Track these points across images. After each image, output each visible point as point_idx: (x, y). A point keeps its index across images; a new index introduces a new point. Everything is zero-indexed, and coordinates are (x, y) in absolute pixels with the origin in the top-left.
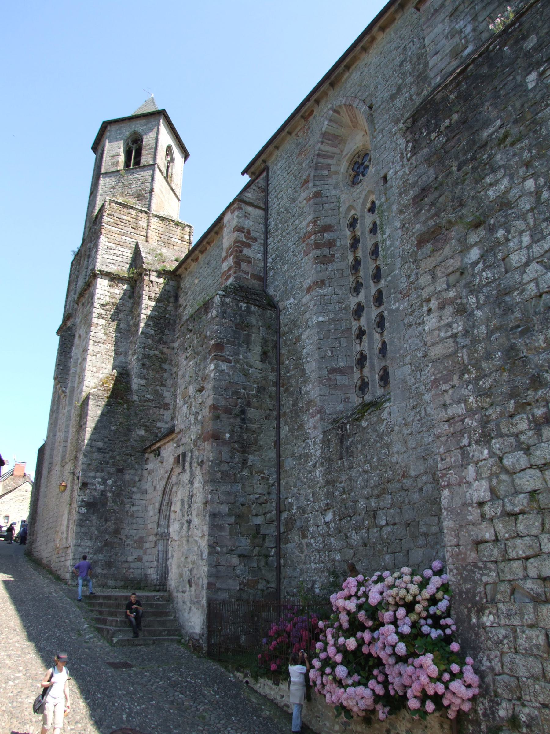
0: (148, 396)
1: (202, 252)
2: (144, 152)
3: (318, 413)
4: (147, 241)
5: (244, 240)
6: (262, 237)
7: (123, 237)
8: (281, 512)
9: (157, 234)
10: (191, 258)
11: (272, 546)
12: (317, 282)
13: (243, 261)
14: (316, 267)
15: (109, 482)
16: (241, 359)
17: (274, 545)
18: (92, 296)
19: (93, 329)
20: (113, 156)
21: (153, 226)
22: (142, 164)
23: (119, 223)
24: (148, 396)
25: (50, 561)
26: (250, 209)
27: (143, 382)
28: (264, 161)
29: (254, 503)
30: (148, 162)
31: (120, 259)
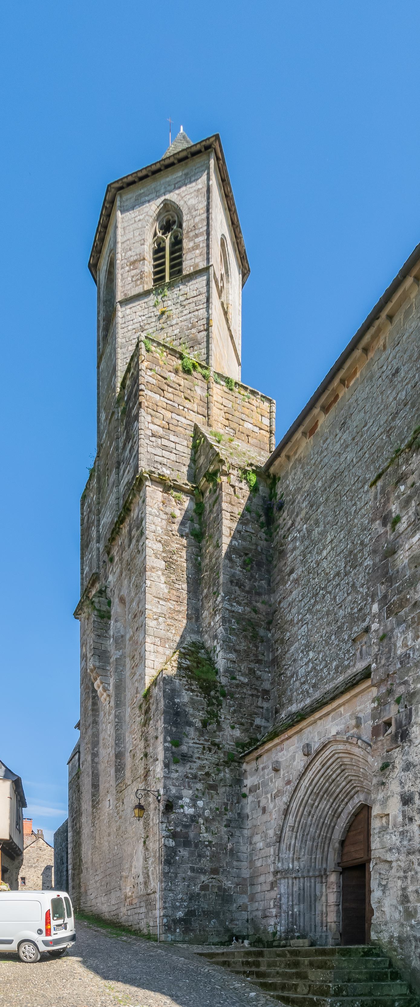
0: (242, 678)
1: (326, 409)
2: (187, 244)
7: (174, 415)
9: (222, 413)
10: (302, 429)
15: (200, 803)
18: (140, 524)
19: (148, 573)
20: (133, 263)
22: (185, 273)
23: (166, 387)
24: (242, 678)
25: (117, 915)
27: (233, 656)
30: (197, 265)
31: (173, 457)
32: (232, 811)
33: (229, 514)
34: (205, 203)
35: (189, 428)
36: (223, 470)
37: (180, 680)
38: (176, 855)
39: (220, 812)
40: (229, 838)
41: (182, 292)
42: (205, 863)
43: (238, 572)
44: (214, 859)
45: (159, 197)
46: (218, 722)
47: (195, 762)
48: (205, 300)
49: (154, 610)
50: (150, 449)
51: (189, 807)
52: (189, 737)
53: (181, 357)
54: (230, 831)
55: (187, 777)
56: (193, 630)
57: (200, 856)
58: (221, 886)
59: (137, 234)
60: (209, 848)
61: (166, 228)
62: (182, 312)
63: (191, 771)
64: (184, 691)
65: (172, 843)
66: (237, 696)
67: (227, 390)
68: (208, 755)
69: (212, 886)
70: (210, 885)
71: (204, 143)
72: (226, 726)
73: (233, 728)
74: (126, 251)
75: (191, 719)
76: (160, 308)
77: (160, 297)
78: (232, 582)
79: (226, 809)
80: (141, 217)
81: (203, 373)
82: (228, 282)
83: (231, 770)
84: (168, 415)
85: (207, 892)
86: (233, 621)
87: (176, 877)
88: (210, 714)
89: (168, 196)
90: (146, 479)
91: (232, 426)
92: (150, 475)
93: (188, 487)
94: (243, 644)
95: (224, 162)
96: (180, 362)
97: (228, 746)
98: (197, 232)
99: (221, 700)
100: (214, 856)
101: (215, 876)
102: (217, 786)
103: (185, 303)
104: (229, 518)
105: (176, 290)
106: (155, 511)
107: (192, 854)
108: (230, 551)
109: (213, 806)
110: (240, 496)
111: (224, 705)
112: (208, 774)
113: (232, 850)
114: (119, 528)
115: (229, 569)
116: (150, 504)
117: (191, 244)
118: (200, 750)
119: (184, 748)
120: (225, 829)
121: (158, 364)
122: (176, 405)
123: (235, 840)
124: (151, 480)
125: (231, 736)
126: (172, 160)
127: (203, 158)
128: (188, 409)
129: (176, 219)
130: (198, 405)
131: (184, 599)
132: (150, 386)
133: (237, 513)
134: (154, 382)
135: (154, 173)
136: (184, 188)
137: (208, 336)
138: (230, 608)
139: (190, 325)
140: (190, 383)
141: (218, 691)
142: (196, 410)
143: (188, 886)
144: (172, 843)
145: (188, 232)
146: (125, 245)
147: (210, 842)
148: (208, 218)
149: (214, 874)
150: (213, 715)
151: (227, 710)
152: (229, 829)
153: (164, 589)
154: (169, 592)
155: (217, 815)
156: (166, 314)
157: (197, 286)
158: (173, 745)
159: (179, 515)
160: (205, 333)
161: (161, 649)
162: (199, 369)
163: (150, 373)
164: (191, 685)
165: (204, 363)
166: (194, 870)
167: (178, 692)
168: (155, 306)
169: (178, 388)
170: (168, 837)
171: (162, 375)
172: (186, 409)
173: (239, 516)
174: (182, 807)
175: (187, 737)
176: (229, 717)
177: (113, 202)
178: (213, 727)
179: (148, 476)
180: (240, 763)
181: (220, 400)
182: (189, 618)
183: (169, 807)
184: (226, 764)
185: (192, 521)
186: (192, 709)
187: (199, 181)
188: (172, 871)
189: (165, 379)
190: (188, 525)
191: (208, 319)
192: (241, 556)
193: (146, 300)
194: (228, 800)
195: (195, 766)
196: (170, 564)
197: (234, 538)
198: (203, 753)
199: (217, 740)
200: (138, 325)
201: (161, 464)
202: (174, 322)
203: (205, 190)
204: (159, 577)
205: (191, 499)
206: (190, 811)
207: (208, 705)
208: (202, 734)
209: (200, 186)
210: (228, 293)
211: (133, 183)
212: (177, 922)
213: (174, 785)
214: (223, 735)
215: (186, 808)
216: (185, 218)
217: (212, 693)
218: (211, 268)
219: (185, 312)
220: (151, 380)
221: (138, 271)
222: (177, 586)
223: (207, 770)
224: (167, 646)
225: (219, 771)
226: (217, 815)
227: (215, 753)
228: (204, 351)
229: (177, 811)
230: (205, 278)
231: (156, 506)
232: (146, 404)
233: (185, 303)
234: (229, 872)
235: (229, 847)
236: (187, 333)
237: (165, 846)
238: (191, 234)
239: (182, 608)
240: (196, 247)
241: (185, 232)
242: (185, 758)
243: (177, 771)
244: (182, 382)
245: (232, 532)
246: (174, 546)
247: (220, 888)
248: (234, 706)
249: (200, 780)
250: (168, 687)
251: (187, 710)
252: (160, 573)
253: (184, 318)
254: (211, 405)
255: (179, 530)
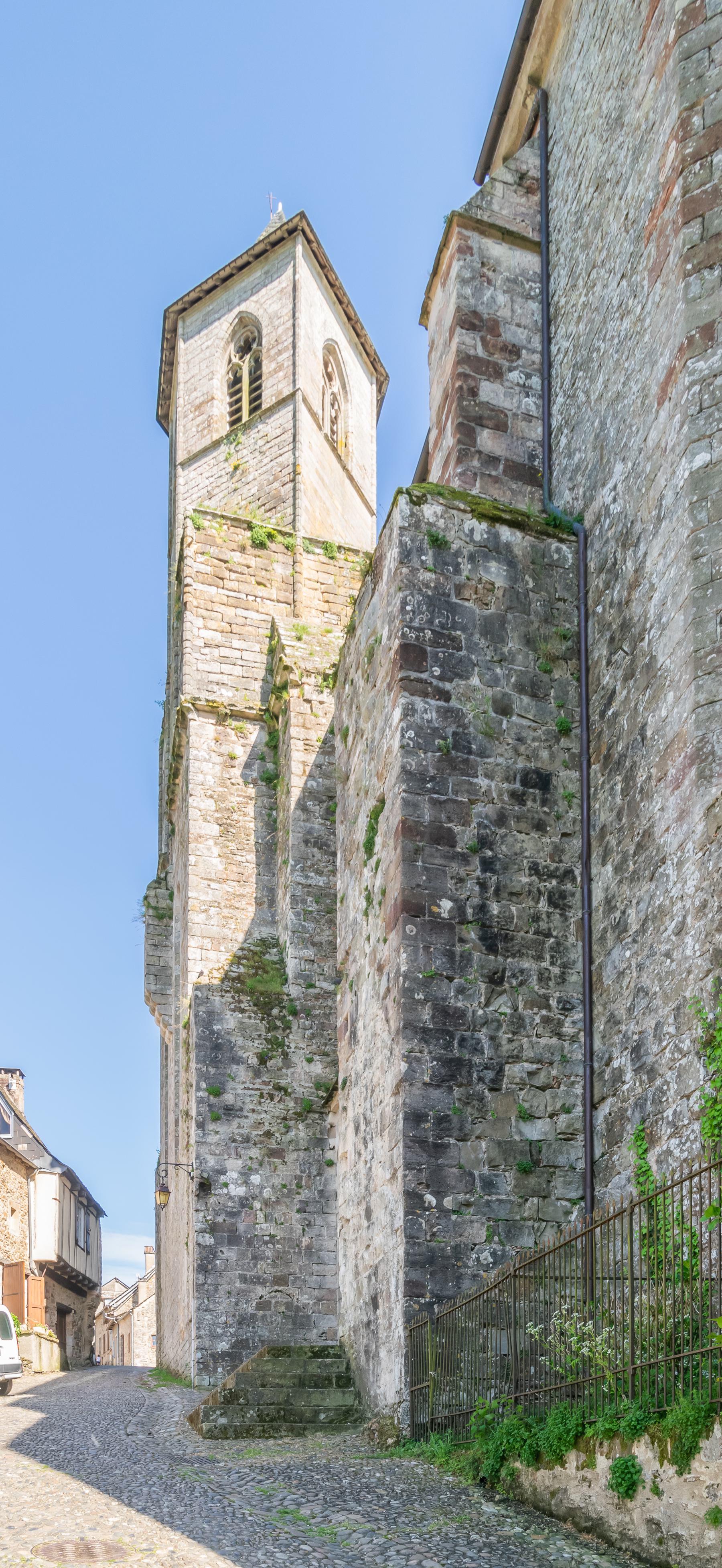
2: (267, 367)
3: (691, 765)
4: (296, 616)
5: (480, 352)
6: (537, 343)
7: (240, 612)
8: (594, 1107)
9: (318, 594)
11: (574, 1195)
12: (691, 339)
13: (480, 421)
14: (687, 286)
15: (255, 1179)
16: (475, 689)
17: (580, 1193)
19: (192, 846)
20: (199, 407)
21: (305, 574)
23: (227, 574)
26: (497, 250)
27: (310, 953)
28: (535, 81)
29: (522, 1085)
30: (280, 392)
31: (238, 671)
32: (308, 1188)
33: (302, 743)
34: (291, 306)
35: (263, 625)
36: (292, 681)
37: (223, 996)
38: (215, 1256)
39: (290, 1191)
40: (304, 1230)
41: (261, 434)
42: (264, 1268)
43: (317, 826)
44: (278, 1262)
45: (230, 310)
46: (285, 1055)
47: (246, 1117)
48: (291, 439)
49: (202, 898)
50: (201, 666)
51: (237, 1184)
52: (237, 1080)
53: (250, 527)
54: (305, 1219)
55: (234, 1141)
56: (264, 920)
57: (255, 1258)
58: (292, 1303)
59: (203, 366)
60: (270, 1246)
61: (245, 349)
62: (261, 461)
63: (240, 1131)
64: (229, 1013)
65: (209, 1240)
66: (317, 1012)
67: (325, 560)
68: (268, 1105)
69: (277, 1302)
70: (273, 1301)
71: (286, 227)
72: (297, 1058)
73: (310, 1061)
74: (189, 392)
75: (240, 1053)
76: (233, 462)
77: (233, 446)
78: (306, 842)
79: (299, 1186)
80: (209, 343)
81: (286, 542)
82: (346, 400)
83: (308, 1126)
84: (230, 612)
85: (268, 1313)
86: (310, 899)
87: (216, 1290)
88: (272, 1044)
89: (243, 307)
90: (189, 709)
91: (333, 610)
92: (193, 704)
93: (254, 712)
94: (327, 933)
95: (319, 244)
96: (249, 534)
97: (302, 1090)
98: (280, 347)
99: (289, 1021)
100: (279, 1258)
101: (280, 1288)
102: (283, 1150)
103: (264, 448)
104: (302, 748)
105: (253, 433)
106: (203, 754)
107: (242, 1255)
108: (304, 797)
109: (277, 1181)
110: (321, 713)
111: (294, 1028)
112: (268, 1134)
113: (309, 1247)
114: (175, 784)
115: (302, 824)
116: (196, 745)
117: (273, 365)
118: (256, 1099)
119: (229, 1098)
120: (298, 1216)
121: (214, 544)
122: (244, 596)
123: (315, 1231)
124: (197, 710)
125: (306, 1073)
126: (245, 258)
127: (289, 244)
128: (262, 598)
129: (256, 334)
130: (279, 589)
131: (250, 876)
132: (201, 576)
133: (315, 739)
134: (209, 569)
135: (225, 280)
136: (264, 291)
137: (294, 489)
138: (303, 881)
139: (271, 478)
140: (266, 561)
141: (284, 1007)
142: (274, 597)
143: (236, 1304)
144: (209, 1240)
145: (269, 350)
146: (189, 384)
147: (272, 1237)
148: (294, 325)
149: (280, 1285)
150: (277, 1044)
151: (300, 1035)
152: (304, 1215)
153: (218, 865)
154: (226, 869)
155: (283, 1195)
156: (241, 468)
157: (280, 421)
158: (210, 1094)
159: (242, 754)
160: (291, 485)
161: (212, 955)
162: (280, 538)
163: (201, 558)
164: (240, 1002)
165: (288, 529)
166: (246, 1279)
167: (219, 1015)
168: (226, 460)
169: (246, 570)
170: (203, 1231)
171: (221, 557)
172: (258, 600)
173: (319, 744)
174: (226, 1185)
175: (233, 1080)
176: (303, 1045)
177: (175, 330)
178: (276, 1062)
179: (190, 705)
180: (322, 1114)
181: (314, 575)
182: (259, 903)
183: (205, 1187)
184: (300, 1116)
185: (263, 759)
186: (241, 1039)
187: (283, 277)
188: (209, 1281)
189: (226, 562)
190: (256, 767)
191: (294, 465)
192: (321, 802)
193: (215, 454)
194: (302, 1171)
195: (246, 1123)
196: (226, 828)
197: (311, 776)
198: (260, 1103)
199: (283, 1083)
200: (205, 491)
201: (218, 684)
202: (251, 477)
203: (290, 288)
204: (209, 849)
205: (262, 728)
206: (239, 1191)
207: (268, 1030)
208: (257, 1073)
209: (284, 285)
210: (347, 417)
211: (199, 299)
212: (217, 1357)
213: (213, 1154)
214: (293, 1074)
215: (232, 1187)
216: (264, 332)
217: (275, 1012)
218: (299, 394)
219: (266, 461)
220: (203, 568)
221: (205, 416)
222: (239, 858)
223: (266, 1127)
224: (222, 949)
225: (288, 1129)
226: (283, 1195)
227: (280, 1101)
228: (290, 510)
229: (217, 1192)
230: (291, 407)
231: (205, 747)
232: (195, 603)
233: (264, 448)
234: (305, 1281)
235: (304, 1244)
236: (267, 489)
237: (199, 1245)
238: (273, 352)
239: (247, 890)
240: (280, 367)
241: (264, 351)
242: (230, 1112)
243: (217, 1133)
244: (252, 562)
245: (308, 769)
246: (234, 800)
247: (288, 1306)
248: (311, 1028)
249: (255, 1144)
250: (202, 1009)
251: (233, 1040)
252: (211, 842)
253: (264, 469)
254: (298, 586)
255: (243, 775)
